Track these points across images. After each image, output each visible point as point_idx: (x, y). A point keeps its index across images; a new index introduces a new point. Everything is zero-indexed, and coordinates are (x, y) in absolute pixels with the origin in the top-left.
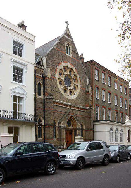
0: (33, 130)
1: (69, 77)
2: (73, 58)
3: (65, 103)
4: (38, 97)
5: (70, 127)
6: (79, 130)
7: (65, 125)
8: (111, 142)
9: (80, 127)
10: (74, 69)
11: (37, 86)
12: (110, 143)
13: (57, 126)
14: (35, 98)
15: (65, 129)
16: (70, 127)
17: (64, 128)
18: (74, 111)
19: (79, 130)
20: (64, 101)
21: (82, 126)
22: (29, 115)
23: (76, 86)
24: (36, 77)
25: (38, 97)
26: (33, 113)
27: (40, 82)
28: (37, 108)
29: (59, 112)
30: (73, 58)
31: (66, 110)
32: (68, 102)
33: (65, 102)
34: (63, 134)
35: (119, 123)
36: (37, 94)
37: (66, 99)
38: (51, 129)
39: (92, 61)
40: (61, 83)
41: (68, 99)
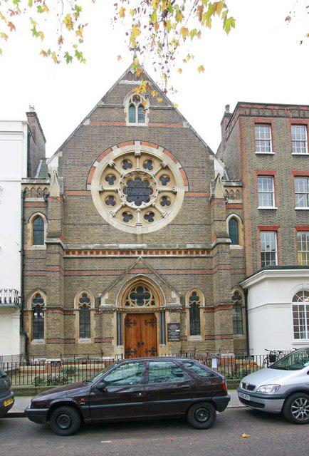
0: (17, 322)
1: (143, 178)
2: (152, 125)
3: (122, 246)
4: (30, 247)
5: (144, 306)
6: (173, 310)
7: (115, 303)
8: (297, 341)
9: (178, 303)
10: (158, 152)
11: (30, 226)
12: (295, 344)
13: (93, 306)
14: (23, 252)
15: (115, 314)
16: (144, 306)
17: (109, 311)
18: (150, 262)
19: (173, 310)
20: (117, 242)
21: (182, 299)
22: (11, 291)
23: (170, 195)
24: (27, 205)
25: (30, 247)
26: (18, 287)
27: (40, 214)
28: (26, 273)
29: (101, 273)
30: (152, 125)
31: (127, 264)
32: (136, 242)
33: (120, 245)
34: (109, 324)
35: (285, 268)
36: (29, 242)
37: (127, 235)
38: (217, 331)
39: (239, 103)
40: (168, 199)
41: (135, 235)
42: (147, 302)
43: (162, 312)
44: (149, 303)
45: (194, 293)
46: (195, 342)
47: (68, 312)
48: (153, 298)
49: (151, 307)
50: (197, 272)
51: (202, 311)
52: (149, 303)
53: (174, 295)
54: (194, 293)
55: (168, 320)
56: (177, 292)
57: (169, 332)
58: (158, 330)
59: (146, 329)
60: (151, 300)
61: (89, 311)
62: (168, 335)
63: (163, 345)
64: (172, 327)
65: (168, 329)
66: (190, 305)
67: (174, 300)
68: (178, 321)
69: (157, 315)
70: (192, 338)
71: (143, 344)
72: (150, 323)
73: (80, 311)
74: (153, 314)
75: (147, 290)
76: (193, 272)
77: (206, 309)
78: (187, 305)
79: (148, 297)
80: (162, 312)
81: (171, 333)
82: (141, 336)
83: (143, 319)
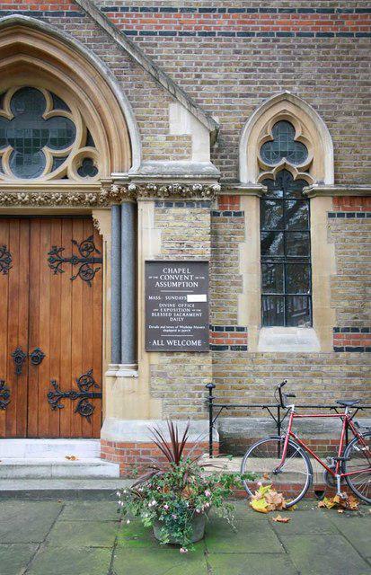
5: (44, 179)
6: (176, 195)
9: (200, 158)
16: (44, 179)
19: (176, 195)
21: (221, 146)
42: (58, 161)
43: (126, 200)
44: (68, 164)
45: (284, 123)
46: (280, 359)
47: (224, 199)
48: (89, 141)
49: (76, 180)
50: (298, 24)
51: (318, 211)
52: (68, 164)
53: (180, 121)
54: (284, 123)
55: (152, 245)
56: (192, 104)
57: (150, 306)
58: (109, 296)
59: (57, 287)
60: (75, 149)
61: (305, 199)
62: (149, 320)
63: (125, 370)
64: (172, 278)
65: (150, 289)
66: (265, 181)
67: (181, 146)
68: (202, 251)
69: (105, 222)
70: (273, 340)
71: (38, 359)
72: (73, 261)
73: (262, 198)
74: (86, 219)
75: (59, 103)
76: (279, 23)
77: (338, 198)
78: (249, 175)
79: (65, 140)
80: (126, 200)
81: (165, 311)
82: (31, 318)
83: (44, 240)
